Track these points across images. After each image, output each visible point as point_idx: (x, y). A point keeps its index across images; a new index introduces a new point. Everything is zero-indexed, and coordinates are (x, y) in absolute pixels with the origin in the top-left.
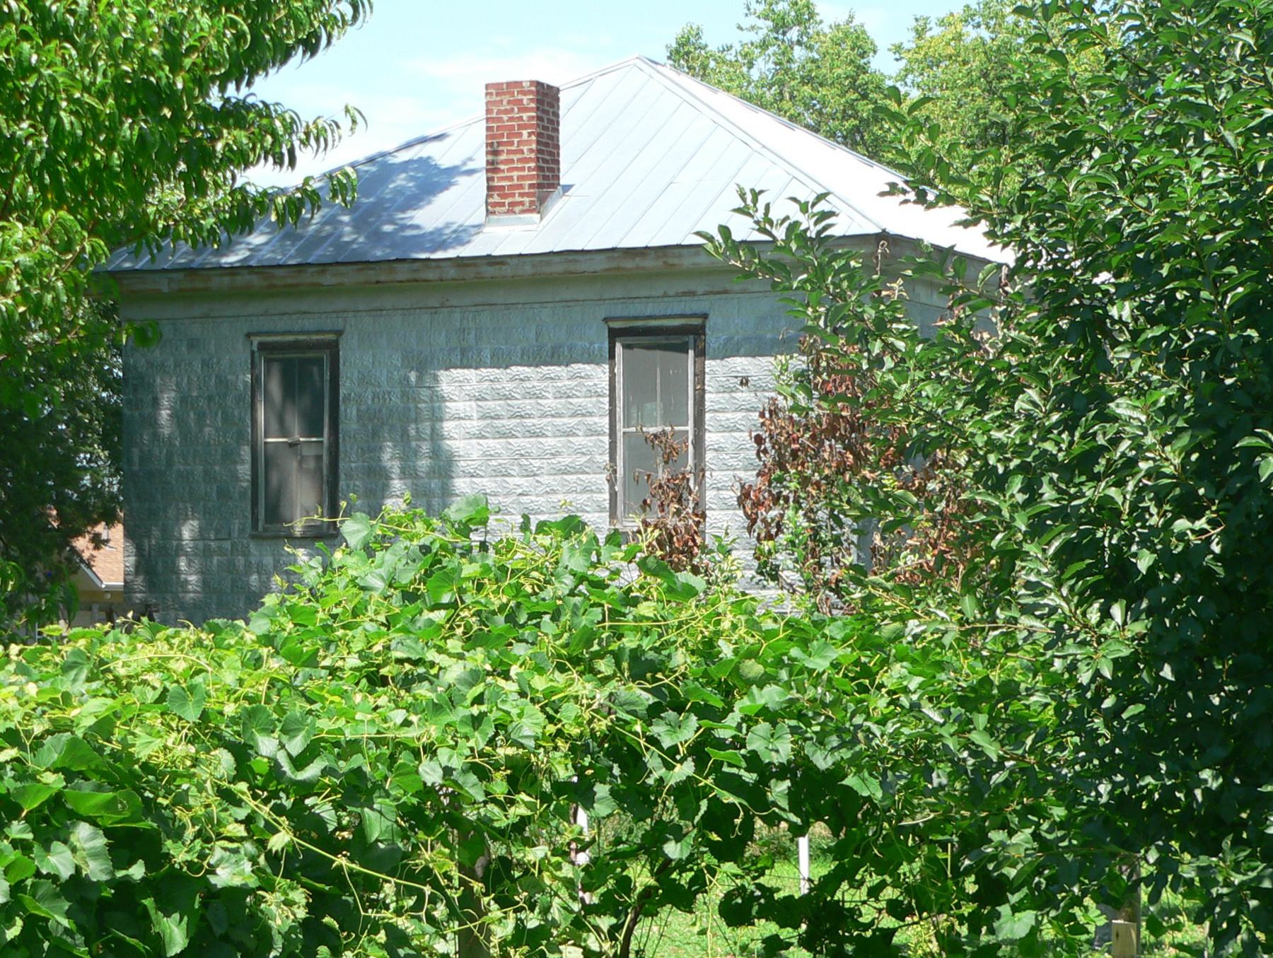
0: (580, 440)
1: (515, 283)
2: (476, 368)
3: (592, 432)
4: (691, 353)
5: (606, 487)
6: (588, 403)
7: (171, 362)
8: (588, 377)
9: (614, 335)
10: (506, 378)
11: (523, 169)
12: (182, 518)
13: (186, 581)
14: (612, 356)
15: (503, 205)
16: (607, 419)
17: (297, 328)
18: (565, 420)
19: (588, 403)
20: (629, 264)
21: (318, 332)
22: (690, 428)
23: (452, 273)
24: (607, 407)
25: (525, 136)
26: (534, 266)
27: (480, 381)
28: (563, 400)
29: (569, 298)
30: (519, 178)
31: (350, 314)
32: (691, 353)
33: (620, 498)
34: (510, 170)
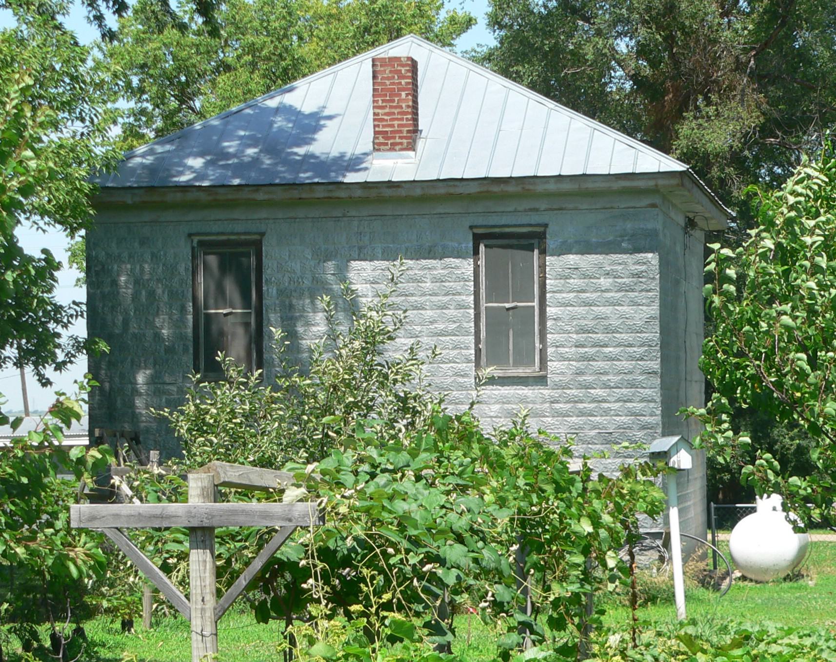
0: (452, 312)
1: (424, 199)
2: (370, 261)
3: (461, 306)
4: (536, 252)
5: (473, 346)
6: (458, 286)
7: (125, 254)
8: (457, 268)
9: (477, 239)
10: (396, 267)
11: (402, 119)
12: (136, 367)
13: (140, 413)
14: (476, 252)
15: (386, 144)
16: (472, 297)
17: (228, 230)
18: (440, 298)
19: (458, 286)
20: (495, 189)
21: (245, 233)
22: (536, 304)
23: (359, 193)
24: (472, 289)
25: (403, 94)
26: (423, 188)
27: (374, 270)
28: (438, 284)
29: (442, 211)
30: (399, 126)
31: (271, 221)
32: (536, 252)
33: (483, 352)
34: (392, 120)
